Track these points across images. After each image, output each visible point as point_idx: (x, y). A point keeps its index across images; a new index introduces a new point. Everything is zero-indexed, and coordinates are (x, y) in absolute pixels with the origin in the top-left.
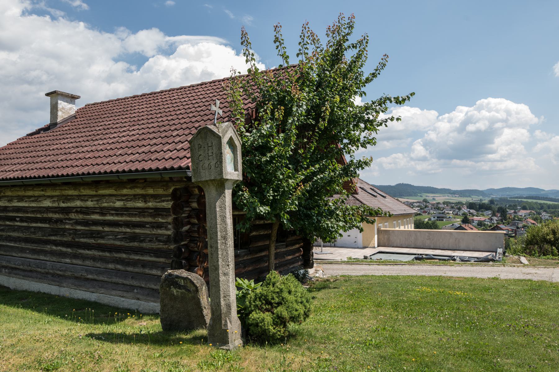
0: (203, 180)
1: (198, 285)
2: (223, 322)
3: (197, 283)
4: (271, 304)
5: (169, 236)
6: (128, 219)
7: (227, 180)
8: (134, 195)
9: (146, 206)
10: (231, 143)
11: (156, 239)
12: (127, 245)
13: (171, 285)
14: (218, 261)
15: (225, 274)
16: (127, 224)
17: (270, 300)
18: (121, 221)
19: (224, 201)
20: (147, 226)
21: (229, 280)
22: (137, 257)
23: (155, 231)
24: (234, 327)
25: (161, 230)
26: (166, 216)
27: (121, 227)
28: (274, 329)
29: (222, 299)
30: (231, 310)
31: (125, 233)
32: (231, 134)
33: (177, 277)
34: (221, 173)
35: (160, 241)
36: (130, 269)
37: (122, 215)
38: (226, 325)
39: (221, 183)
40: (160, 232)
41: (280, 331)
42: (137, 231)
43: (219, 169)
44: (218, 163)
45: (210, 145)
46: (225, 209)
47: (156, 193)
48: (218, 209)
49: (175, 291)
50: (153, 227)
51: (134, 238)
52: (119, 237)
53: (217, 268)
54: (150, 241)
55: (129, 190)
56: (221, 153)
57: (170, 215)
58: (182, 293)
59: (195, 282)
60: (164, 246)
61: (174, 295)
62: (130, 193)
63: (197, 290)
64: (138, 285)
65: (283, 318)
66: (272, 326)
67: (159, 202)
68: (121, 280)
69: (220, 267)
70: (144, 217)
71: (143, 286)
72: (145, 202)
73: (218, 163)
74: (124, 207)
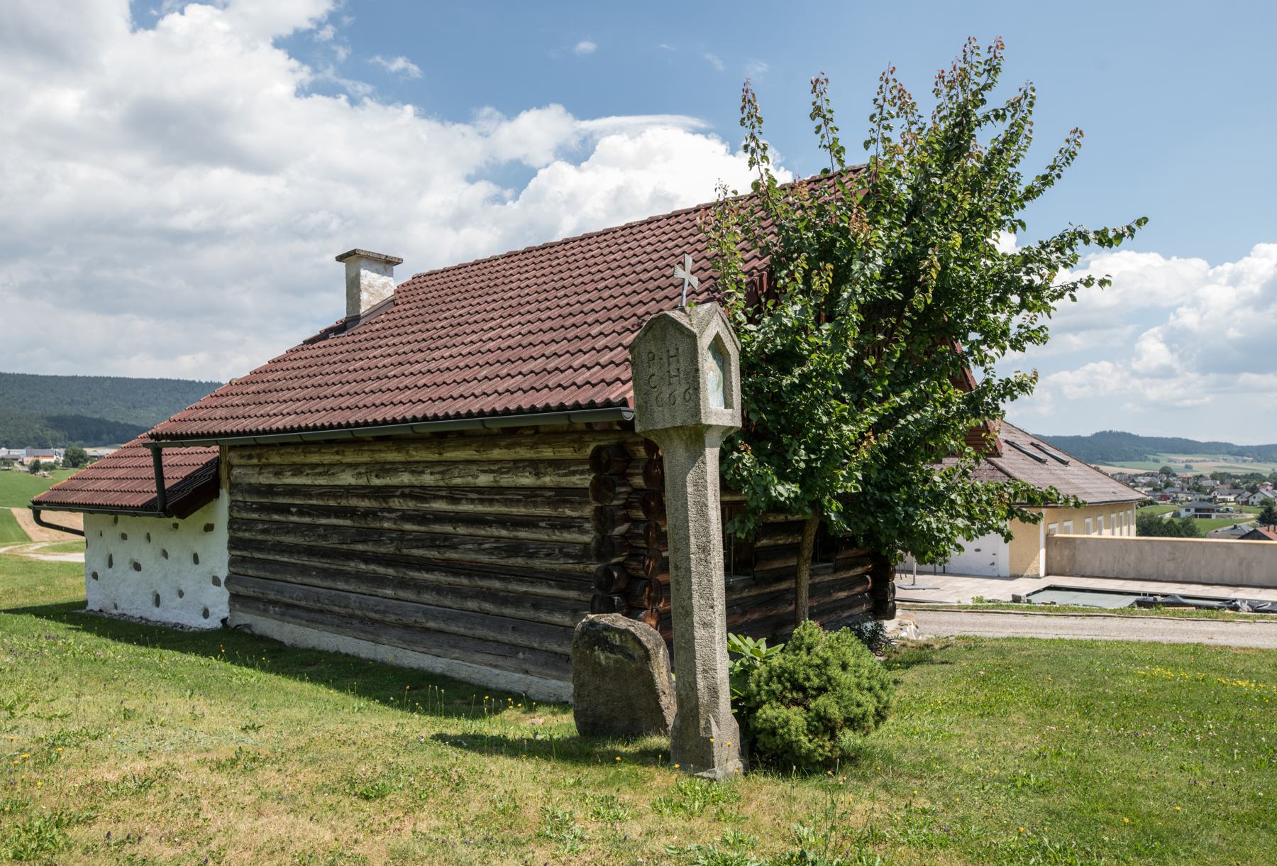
0: (659, 427)
1: (649, 647)
2: (702, 722)
3: (648, 641)
4: (803, 689)
5: (586, 544)
6: (504, 509)
7: (710, 426)
8: (515, 462)
9: (539, 483)
11: (560, 551)
12: (502, 562)
14: (690, 598)
15: (706, 625)
16: (502, 521)
18: (489, 514)
19: (704, 472)
22: (522, 588)
23: (557, 536)
24: (724, 734)
26: (580, 503)
28: (810, 741)
29: (699, 676)
31: (498, 539)
32: (718, 329)
33: (607, 628)
34: (697, 412)
35: (567, 555)
36: (509, 611)
37: (491, 502)
40: (567, 536)
41: (822, 747)
42: (523, 534)
43: (691, 404)
44: (691, 391)
45: (672, 353)
47: (558, 456)
49: (602, 657)
50: (553, 527)
51: (516, 548)
52: (487, 546)
53: (688, 613)
54: (548, 555)
55: (504, 451)
56: (697, 370)
57: (589, 503)
58: (616, 661)
59: (643, 639)
61: (600, 664)
62: (507, 458)
63: (647, 656)
65: (830, 720)
67: (565, 475)
69: (696, 609)
70: (535, 506)
71: (536, 645)
73: (691, 391)
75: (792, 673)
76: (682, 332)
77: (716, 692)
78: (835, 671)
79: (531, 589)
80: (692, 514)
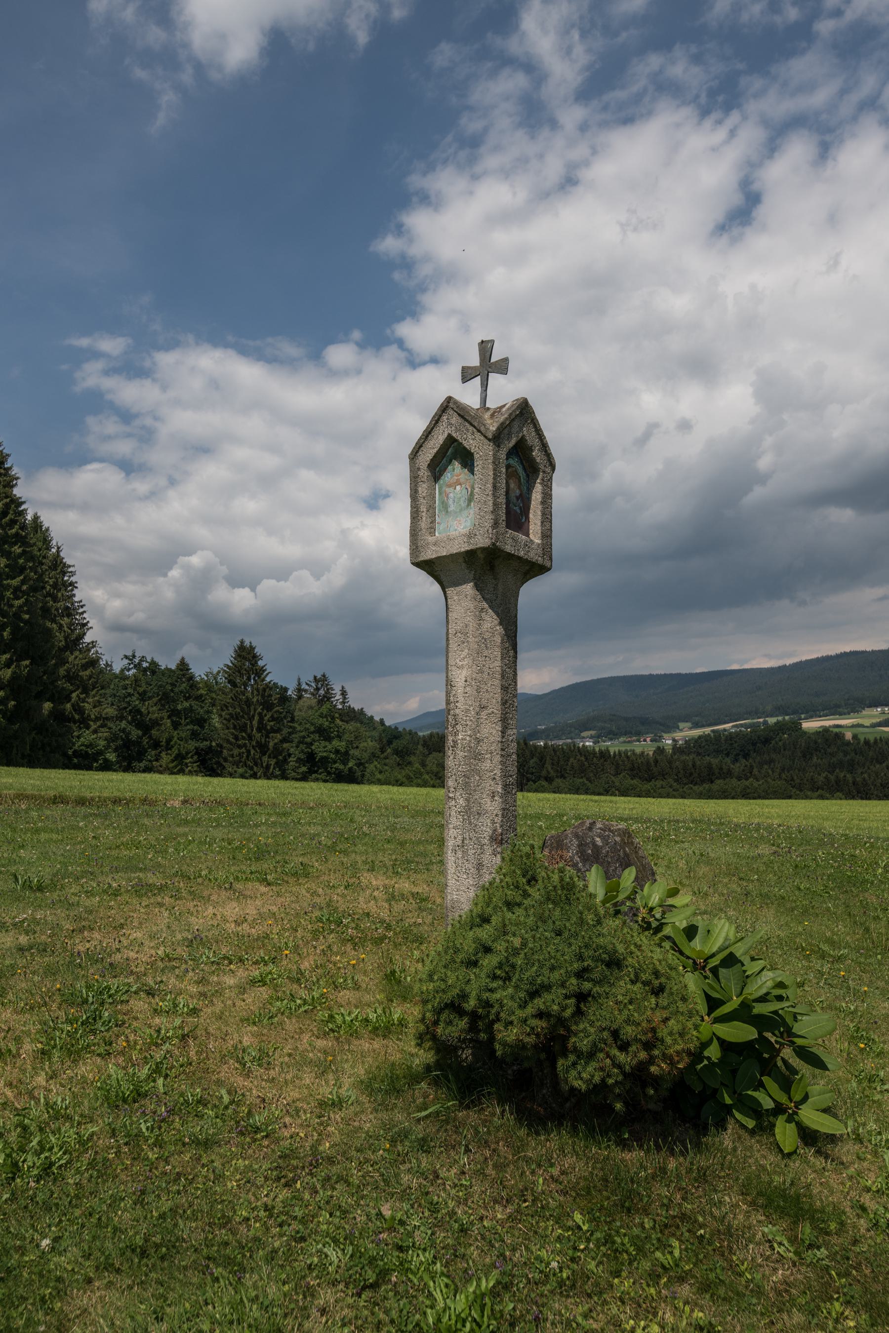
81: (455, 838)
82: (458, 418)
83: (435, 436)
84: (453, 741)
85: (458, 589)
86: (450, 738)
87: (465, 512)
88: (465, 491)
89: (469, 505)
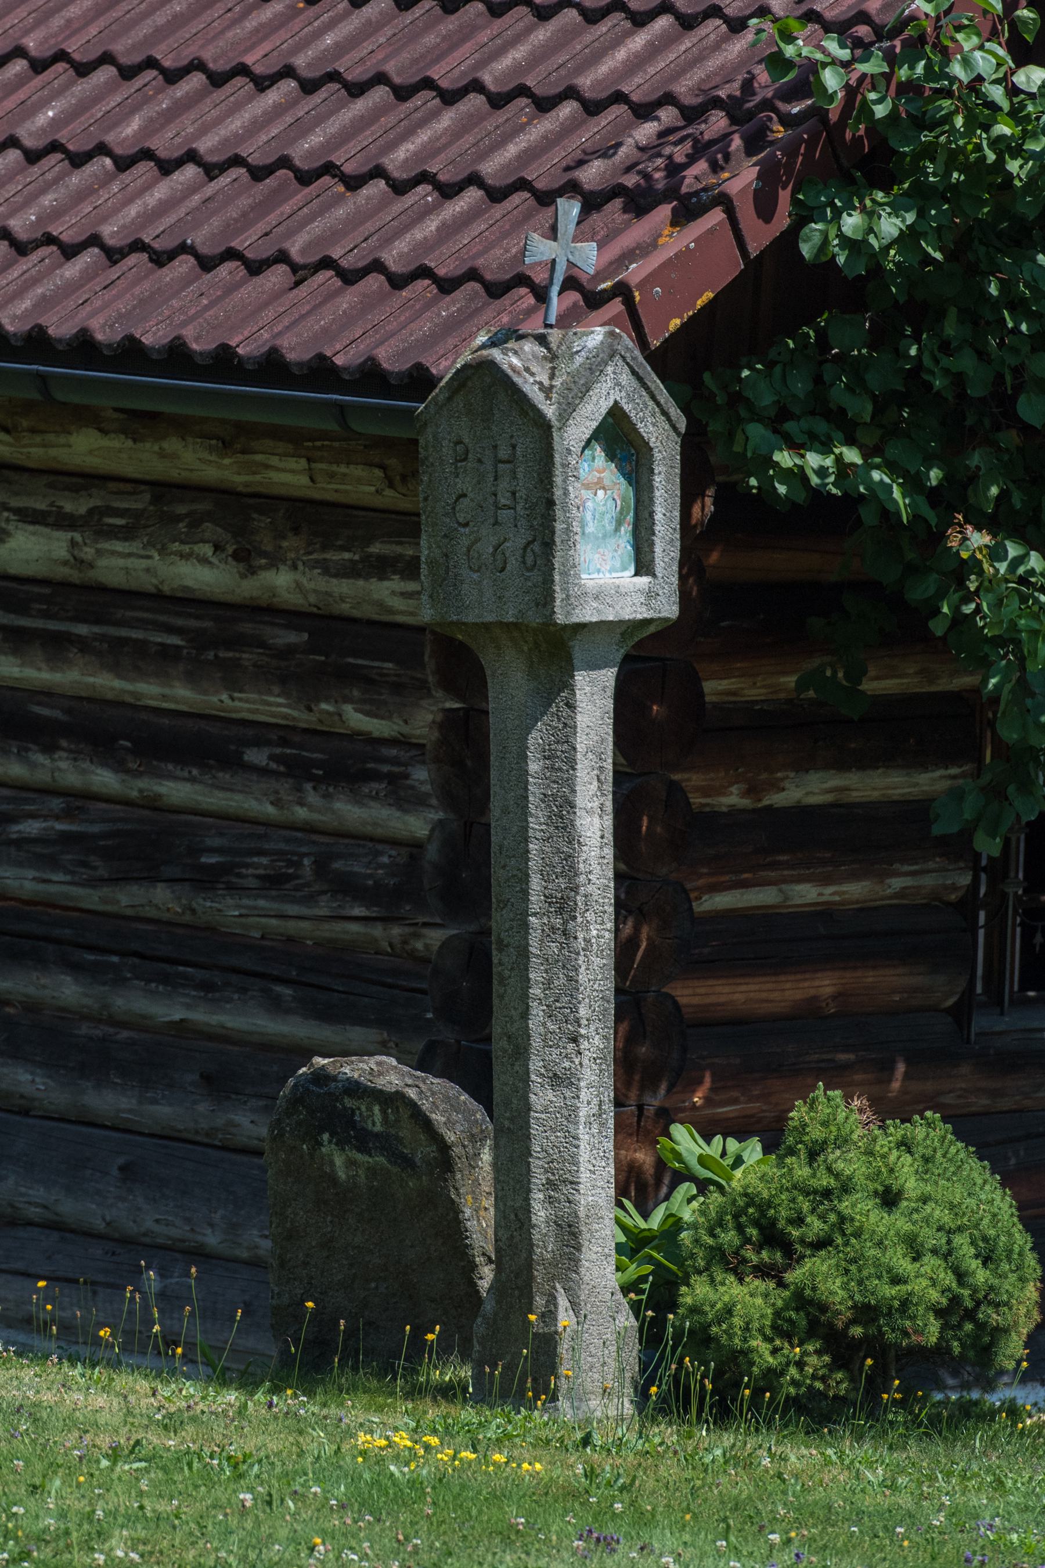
0: (471, 618)
1: (450, 1137)
2: (539, 1301)
3: (450, 1124)
4: (785, 1246)
5: (416, 846)
6: (107, 683)
7: (581, 627)
8: (163, 490)
9: (249, 588)
10: (617, 437)
11: (321, 867)
12: (91, 898)
13: (322, 1130)
14: (525, 1015)
15: (561, 1080)
16: (97, 730)
17: (781, 1224)
18: (46, 694)
19: (570, 727)
20: (256, 756)
21: (576, 1110)
22: (171, 1010)
23: (313, 807)
24: (595, 1325)
25: (358, 800)
26: (397, 688)
27: (50, 749)
28: (775, 1351)
29: (537, 1196)
30: (578, 1248)
31: (79, 801)
32: (616, 395)
33: (354, 1089)
34: (546, 598)
35: (346, 887)
36: (110, 1101)
37: (56, 646)
38: (549, 1315)
39: (556, 650)
40: (350, 812)
41: (800, 1365)
42: (177, 790)
43: (536, 576)
44: (536, 547)
45: (503, 453)
46: (572, 764)
47: (326, 491)
48: (534, 767)
49: (339, 1161)
50: (298, 771)
51: (149, 844)
52: (32, 827)
53: (521, 1051)
54: (273, 882)
55: (115, 442)
56: (551, 503)
57: (422, 688)
58: (372, 1172)
59: (438, 1118)
60: (377, 931)
61: (333, 1179)
62: (129, 469)
63: (444, 1161)
64: (178, 1231)
65: (823, 1308)
66: (768, 1339)
67: (350, 571)
68: (39, 1193)
69: (536, 1042)
70: (233, 685)
71: (212, 1239)
72: (246, 558)
73: (536, 547)
74: (74, 576)
75: (764, 1206)
76: (524, 413)
77: (575, 1235)
78: (862, 1208)
79: (202, 1016)
80: (537, 822)
81: (589, 1103)
82: (630, 377)
83: (594, 399)
84: (585, 940)
85: (594, 674)
86: (581, 935)
87: (612, 542)
88: (610, 502)
89: (617, 530)
